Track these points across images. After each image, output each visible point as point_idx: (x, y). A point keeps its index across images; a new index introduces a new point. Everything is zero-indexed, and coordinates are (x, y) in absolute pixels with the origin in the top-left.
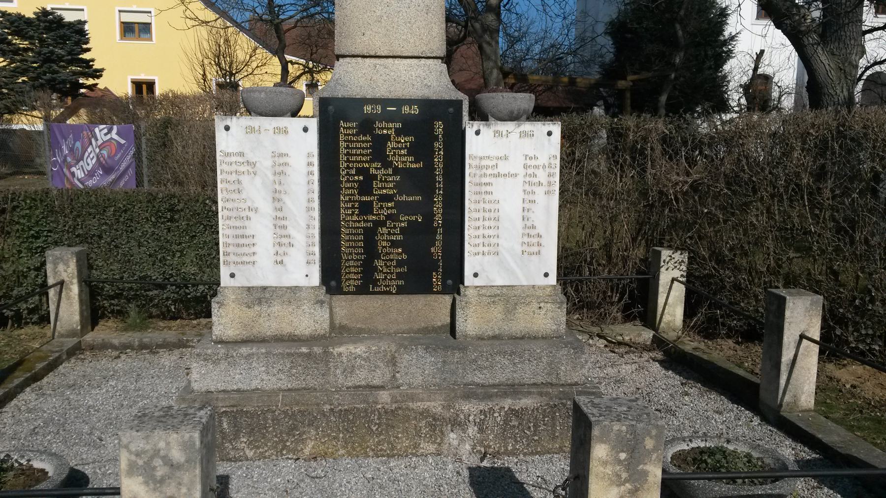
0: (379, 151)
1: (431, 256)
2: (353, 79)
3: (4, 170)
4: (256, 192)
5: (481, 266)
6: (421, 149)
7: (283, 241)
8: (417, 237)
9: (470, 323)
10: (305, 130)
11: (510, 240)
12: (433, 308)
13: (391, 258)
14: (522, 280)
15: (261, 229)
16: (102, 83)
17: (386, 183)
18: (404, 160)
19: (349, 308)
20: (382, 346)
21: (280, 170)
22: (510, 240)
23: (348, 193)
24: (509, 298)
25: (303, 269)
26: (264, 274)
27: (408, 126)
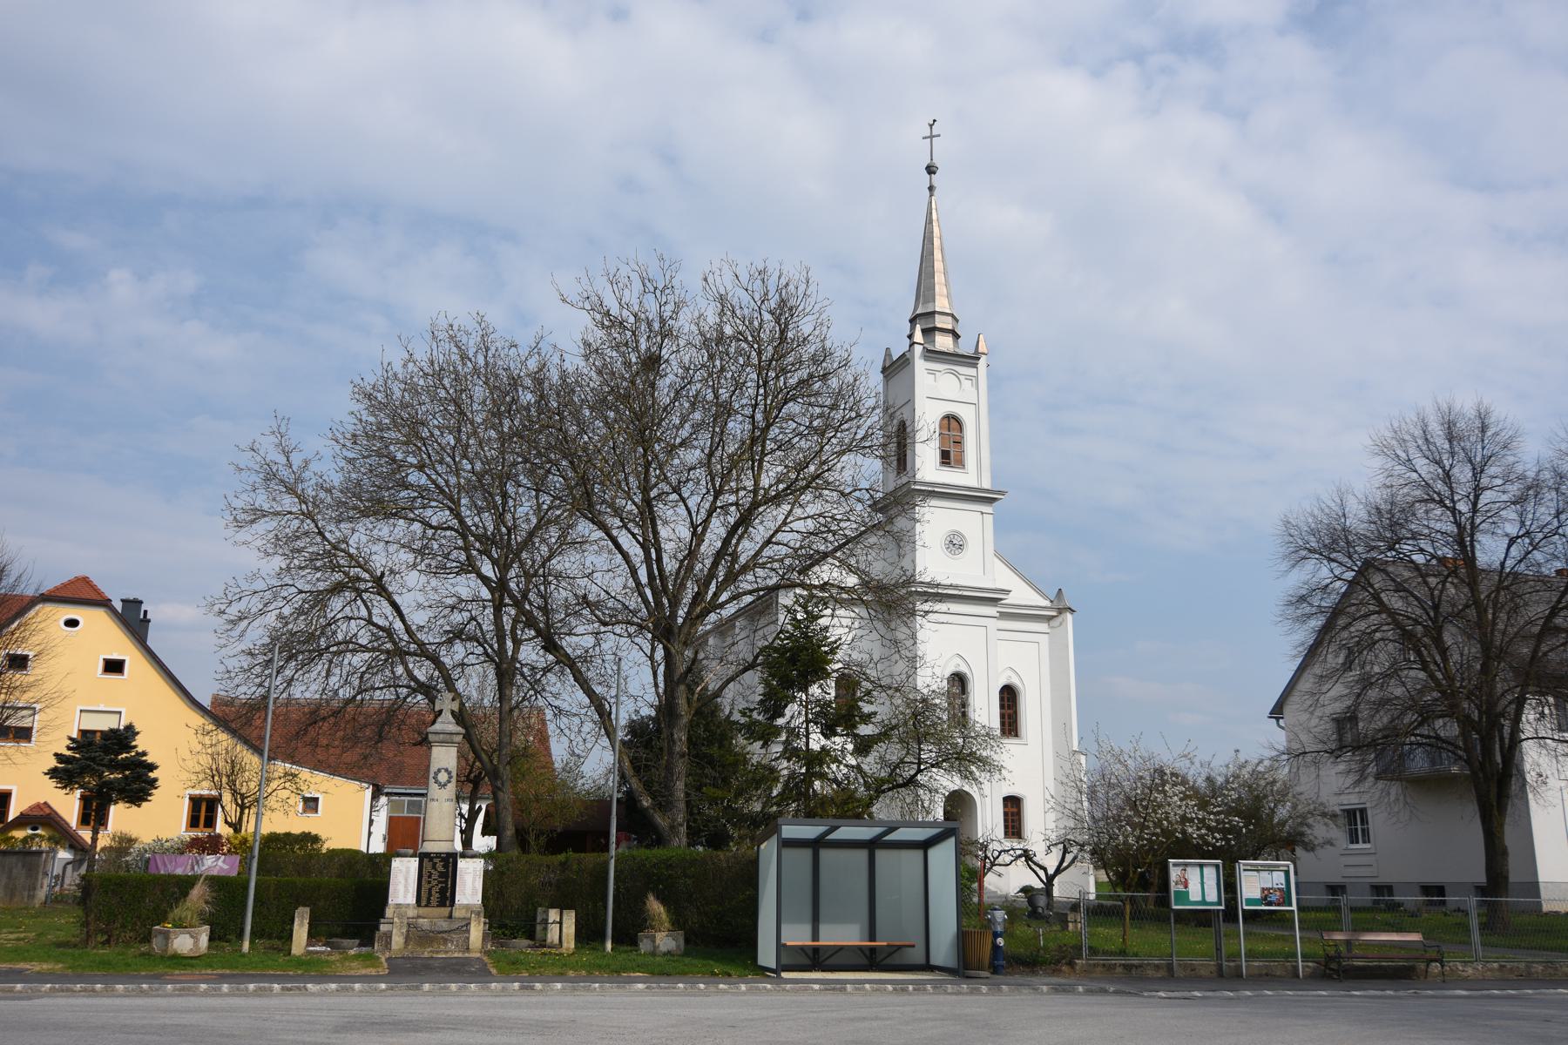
0: (434, 867)
1: (446, 895)
2: (429, 847)
3: (8, 937)
4: (401, 878)
5: (461, 899)
6: (446, 866)
7: (406, 891)
8: (442, 892)
9: (456, 914)
10: (72, 623)
11: (469, 891)
12: (445, 911)
13: (435, 896)
14: (471, 902)
15: (401, 888)
16: (329, 845)
17: (435, 875)
18: (440, 869)
19: (422, 911)
20: (432, 918)
21: (408, 872)
22: (469, 891)
23: (425, 878)
24: (467, 907)
25: (411, 899)
26: (400, 901)
27: (443, 860)
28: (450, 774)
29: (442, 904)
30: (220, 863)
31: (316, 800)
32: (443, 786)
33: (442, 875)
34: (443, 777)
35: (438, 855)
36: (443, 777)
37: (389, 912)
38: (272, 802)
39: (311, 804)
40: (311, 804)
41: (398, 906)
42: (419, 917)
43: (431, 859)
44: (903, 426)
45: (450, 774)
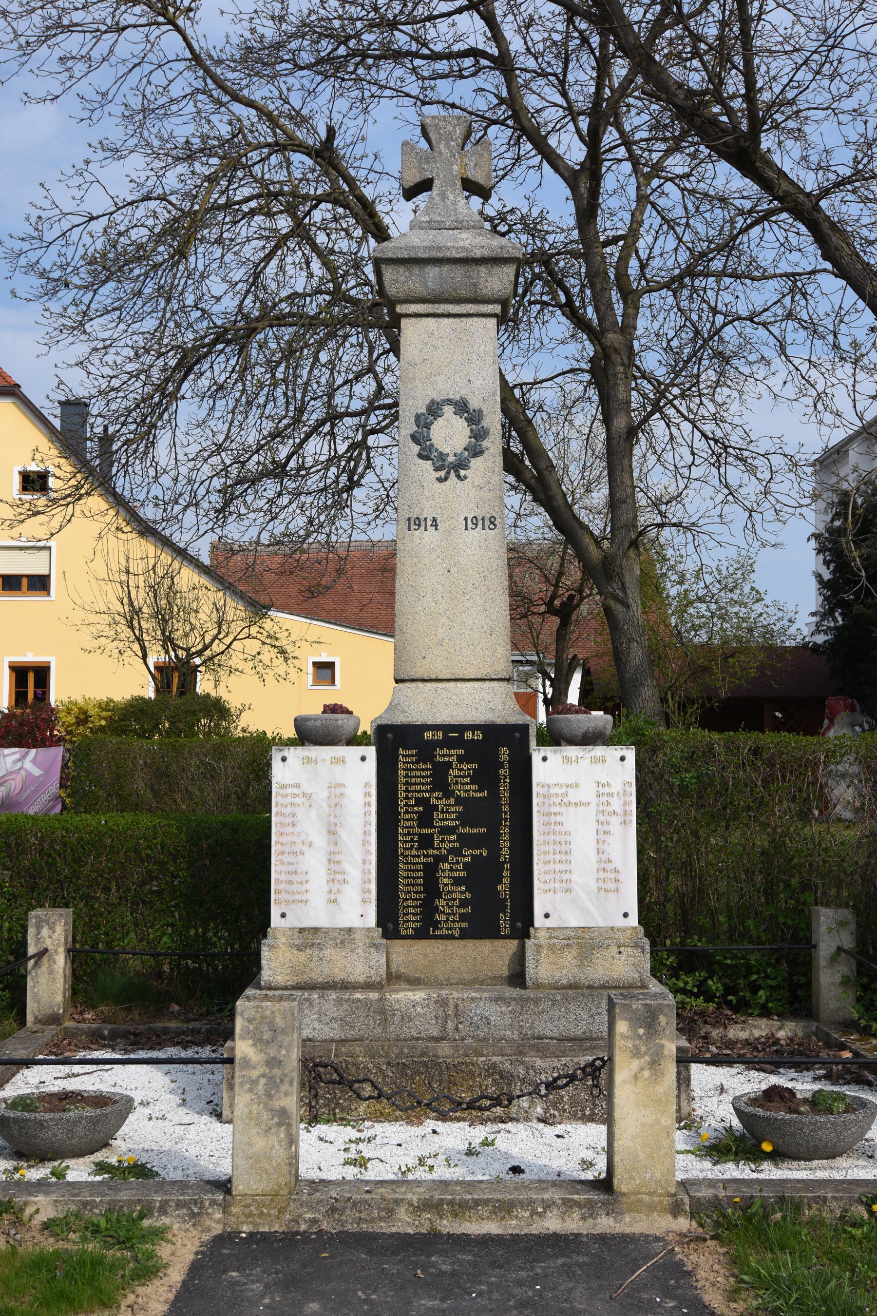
5: (557, 904)
6: (486, 777)
7: (336, 876)
8: (481, 876)
9: (542, 967)
12: (496, 954)
13: (453, 897)
15: (315, 866)
17: (447, 813)
18: (465, 788)
19: (409, 954)
20: (445, 987)
21: (336, 802)
25: (359, 909)
26: (317, 915)
27: (472, 752)
28: (473, 418)
29: (481, 927)
30: (28, 765)
31: (331, 666)
32: (453, 468)
33: (471, 812)
34: (451, 434)
35: (453, 734)
36: (451, 434)
37: (276, 962)
38: (236, 660)
39: (325, 670)
40: (325, 670)
41: (310, 937)
42: (394, 978)
43: (426, 751)
44: (209, 1182)
45: (473, 418)
